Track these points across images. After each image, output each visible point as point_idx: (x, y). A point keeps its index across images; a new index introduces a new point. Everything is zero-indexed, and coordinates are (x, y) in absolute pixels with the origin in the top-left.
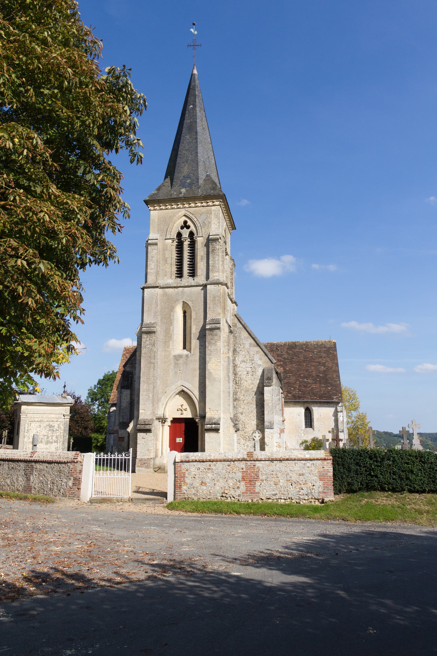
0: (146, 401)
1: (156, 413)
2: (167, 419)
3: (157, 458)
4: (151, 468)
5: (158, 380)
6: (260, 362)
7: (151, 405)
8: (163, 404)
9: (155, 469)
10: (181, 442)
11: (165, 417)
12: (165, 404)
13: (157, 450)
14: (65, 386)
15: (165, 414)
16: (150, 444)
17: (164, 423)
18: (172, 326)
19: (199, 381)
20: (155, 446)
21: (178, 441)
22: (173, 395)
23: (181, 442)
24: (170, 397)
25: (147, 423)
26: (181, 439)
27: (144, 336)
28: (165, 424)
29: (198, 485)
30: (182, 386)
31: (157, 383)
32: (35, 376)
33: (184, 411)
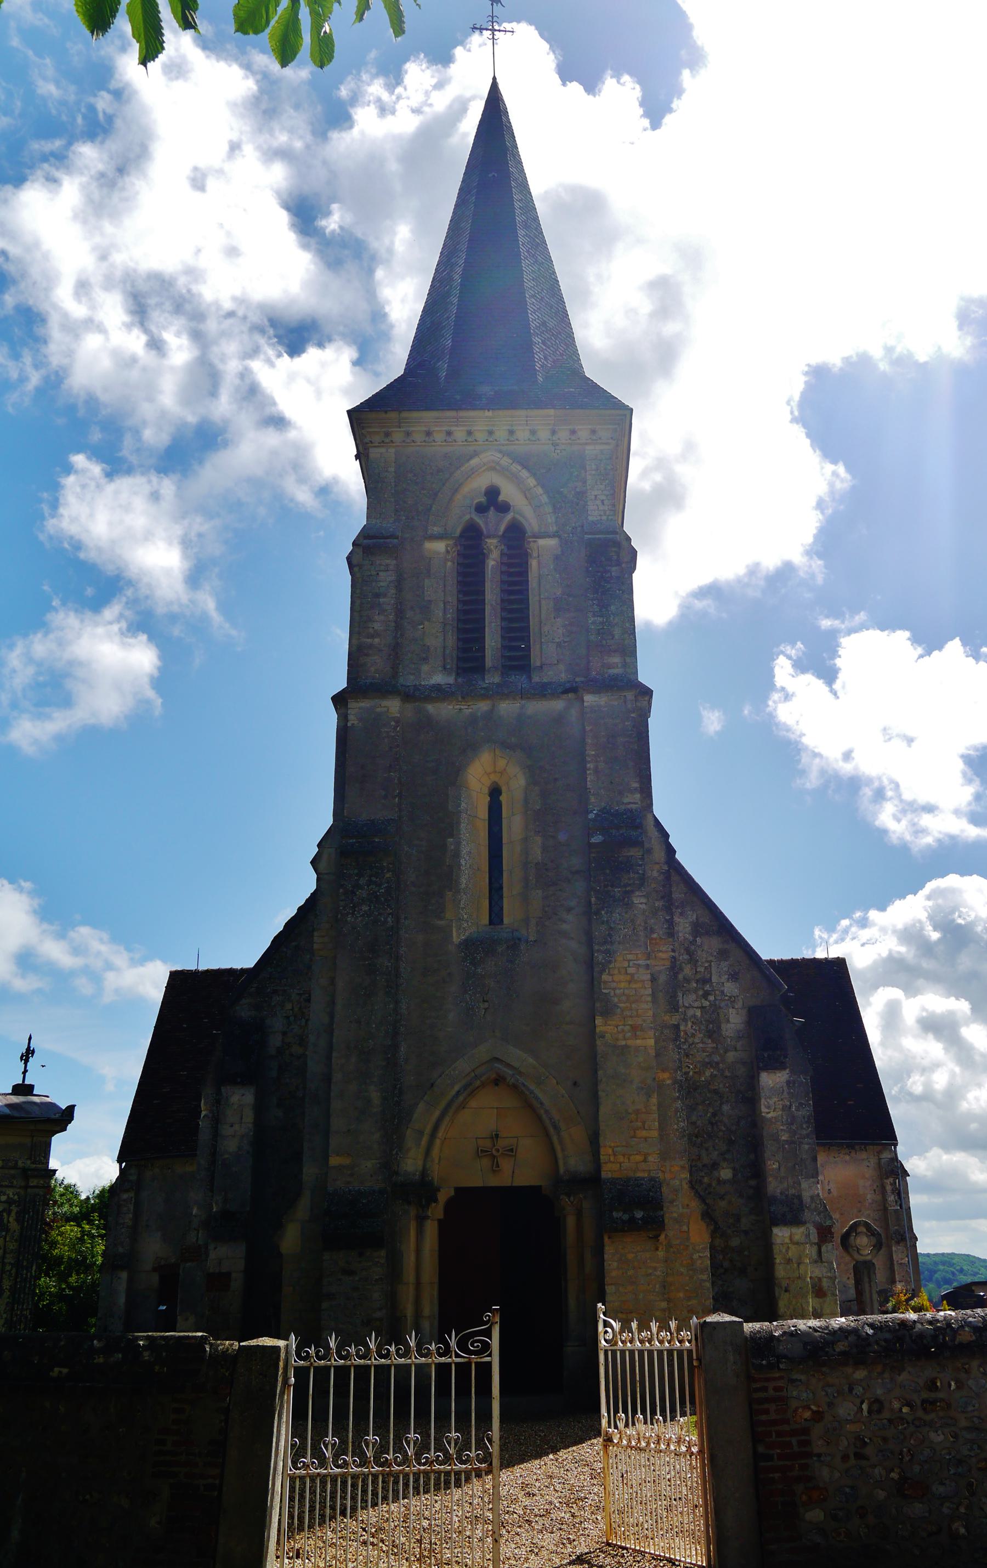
6: (730, 988)
8: (421, 1133)
12: (428, 1130)
14: (28, 1054)
18: (451, 835)
24: (449, 1105)
29: (881, 1495)
32: (487, 540)
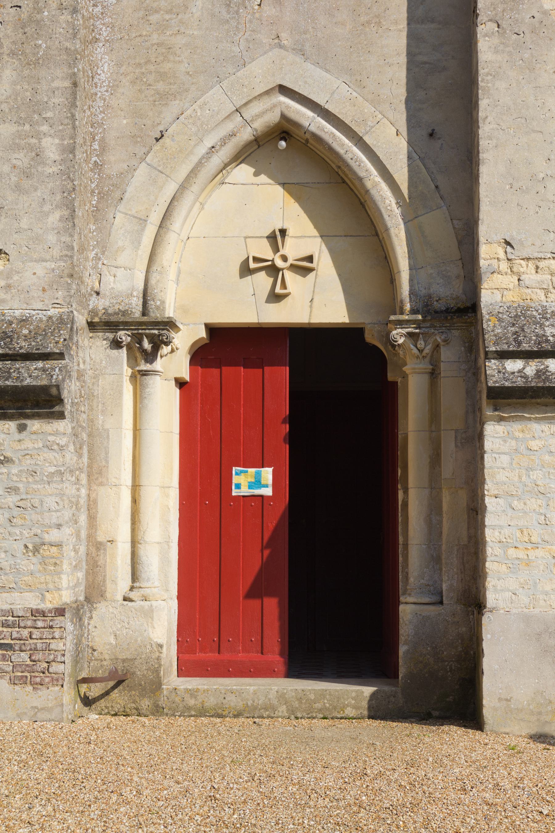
0: (18, 188)
1: (92, 282)
2: (170, 324)
3: (102, 608)
4: (58, 681)
5: (100, 49)
7: (54, 218)
8: (143, 221)
9: (84, 688)
10: (268, 492)
11: (154, 315)
12: (155, 218)
13: (99, 546)
15: (155, 291)
16: (50, 502)
17: (150, 357)
19: (411, 55)
20: (83, 519)
21: (245, 491)
22: (217, 161)
23: (268, 492)
25: (22, 346)
26: (267, 473)
27: (13, 637)
28: (158, 365)
30: (283, 90)
31: (93, 65)
33: (289, 276)
